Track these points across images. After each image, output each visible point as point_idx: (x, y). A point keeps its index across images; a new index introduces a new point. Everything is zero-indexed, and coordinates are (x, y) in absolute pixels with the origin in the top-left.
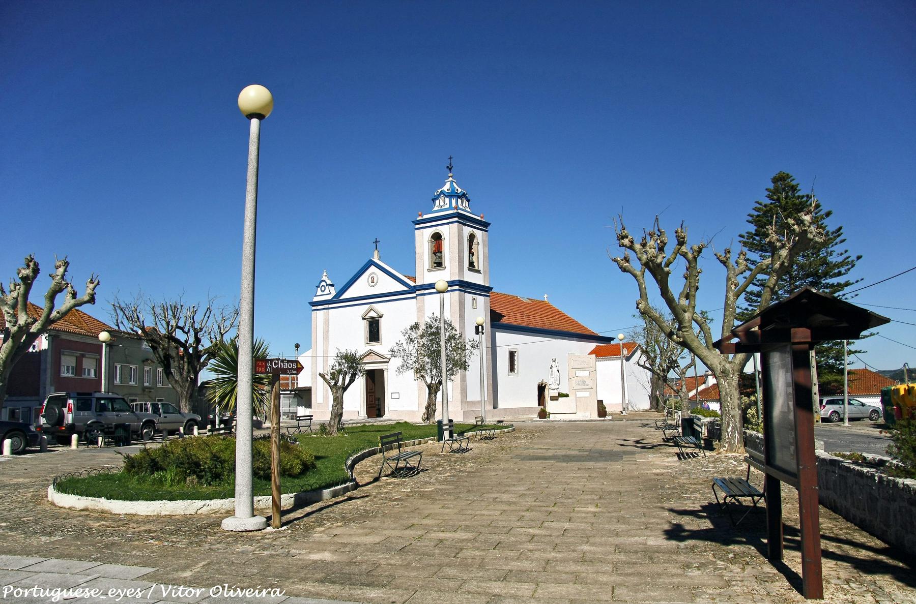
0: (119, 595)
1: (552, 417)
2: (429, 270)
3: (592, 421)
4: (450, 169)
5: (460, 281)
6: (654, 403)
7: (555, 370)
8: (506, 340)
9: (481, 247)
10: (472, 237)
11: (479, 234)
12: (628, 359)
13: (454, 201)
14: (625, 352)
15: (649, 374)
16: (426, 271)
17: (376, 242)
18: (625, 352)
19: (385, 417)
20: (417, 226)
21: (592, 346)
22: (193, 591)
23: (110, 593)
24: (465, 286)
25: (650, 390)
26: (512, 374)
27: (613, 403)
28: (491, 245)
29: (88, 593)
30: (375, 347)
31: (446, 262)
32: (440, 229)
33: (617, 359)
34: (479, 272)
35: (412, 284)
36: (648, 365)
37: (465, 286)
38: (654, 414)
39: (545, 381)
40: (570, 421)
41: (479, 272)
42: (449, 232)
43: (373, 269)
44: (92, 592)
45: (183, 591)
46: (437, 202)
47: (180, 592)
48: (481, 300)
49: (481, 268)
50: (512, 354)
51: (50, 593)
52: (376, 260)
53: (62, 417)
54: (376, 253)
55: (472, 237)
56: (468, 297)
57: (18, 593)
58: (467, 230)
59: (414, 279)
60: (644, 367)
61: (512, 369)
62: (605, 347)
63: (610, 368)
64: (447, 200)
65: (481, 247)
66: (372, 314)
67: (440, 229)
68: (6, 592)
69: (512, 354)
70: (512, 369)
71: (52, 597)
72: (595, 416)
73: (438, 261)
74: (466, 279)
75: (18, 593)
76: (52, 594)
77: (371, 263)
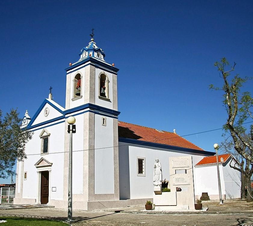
1: (157, 209)
4: (92, 36)
5: (90, 104)
6: (244, 194)
7: (158, 169)
8: (135, 152)
9: (111, 84)
10: (103, 78)
11: (110, 76)
12: (224, 165)
13: (91, 53)
14: (222, 160)
17: (51, 88)
18: (222, 160)
20: (68, 72)
21: (201, 158)
24: (94, 108)
26: (140, 175)
27: (214, 194)
30: (45, 156)
31: (83, 93)
32: (80, 71)
34: (108, 100)
35: (63, 110)
37: (94, 108)
39: (167, 181)
40: (170, 213)
41: (108, 100)
42: (85, 71)
43: (47, 105)
46: (82, 56)
48: (110, 120)
49: (111, 98)
50: (140, 162)
52: (49, 100)
54: (50, 95)
55: (103, 78)
56: (99, 118)
61: (140, 171)
62: (209, 157)
64: (87, 53)
65: (111, 84)
66: (45, 134)
67: (80, 71)
69: (140, 162)
70: (140, 171)
72: (193, 209)
73: (78, 92)
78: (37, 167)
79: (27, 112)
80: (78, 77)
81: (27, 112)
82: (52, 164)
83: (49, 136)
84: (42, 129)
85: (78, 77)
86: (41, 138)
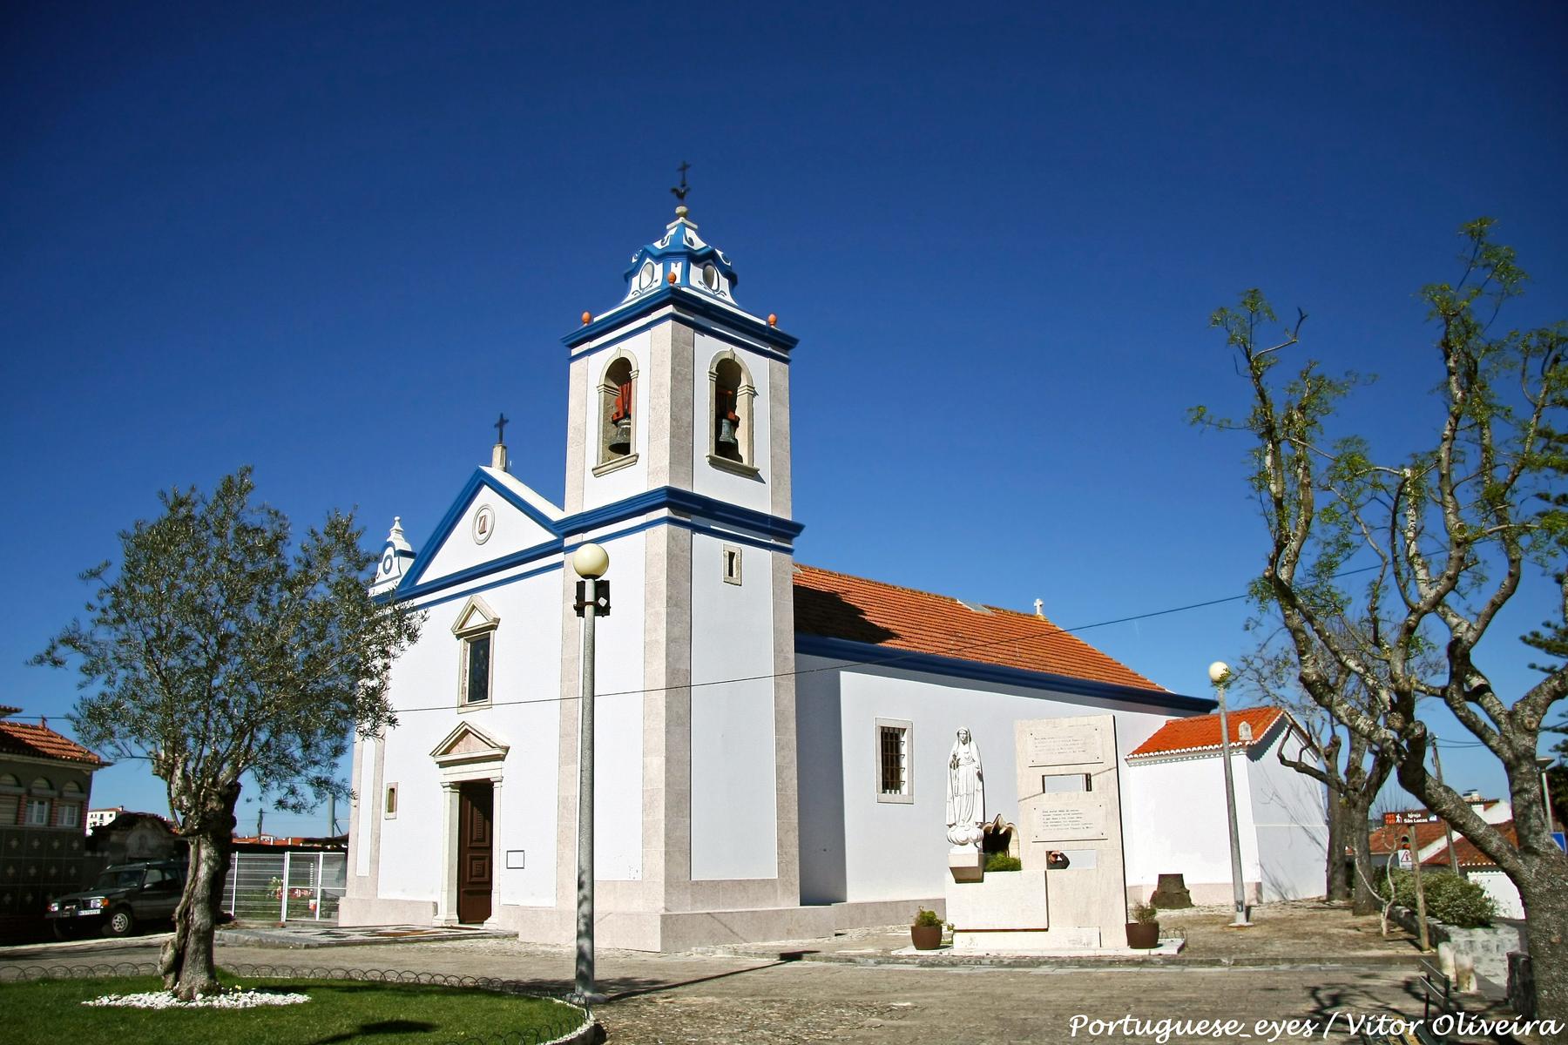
0: (1272, 1034)
2: (597, 472)
3: (1098, 962)
6: (1340, 879)
7: (967, 772)
8: (868, 699)
9: (763, 404)
10: (727, 378)
11: (758, 369)
12: (1255, 753)
15: (1319, 787)
16: (589, 474)
19: (490, 924)
20: (575, 352)
21: (1156, 722)
22: (1103, 1025)
23: (1257, 1028)
25: (1325, 840)
26: (888, 796)
27: (1209, 881)
28: (803, 406)
29: (1219, 1029)
30: (478, 717)
31: (639, 444)
32: (627, 349)
33: (1213, 753)
34: (752, 474)
35: (555, 514)
36: (1309, 759)
38: (1342, 921)
40: (1018, 962)
41: (752, 474)
44: (1227, 1027)
45: (1387, 1025)
46: (635, 280)
47: (1380, 1027)
48: (758, 561)
49: (763, 464)
50: (890, 740)
51: (1152, 1027)
52: (495, 471)
53: (156, 885)
54: (498, 452)
55: (727, 378)
56: (709, 549)
57: (1097, 1028)
58: (709, 350)
59: (560, 503)
60: (1301, 768)
61: (891, 779)
62: (1189, 719)
63: (1198, 774)
64: (659, 268)
65: (763, 404)
66: (476, 621)
67: (627, 349)
68: (1075, 1027)
69: (890, 740)
70: (891, 779)
71: (1156, 1034)
72: (1117, 944)
74: (699, 490)
75: (1097, 1028)
76: (1157, 1029)
77: (484, 480)
78: (442, 765)
79: (397, 526)
80: (621, 373)
81: (397, 526)
82: (507, 749)
83: (494, 627)
84: (466, 599)
85: (621, 373)
86: (459, 636)
